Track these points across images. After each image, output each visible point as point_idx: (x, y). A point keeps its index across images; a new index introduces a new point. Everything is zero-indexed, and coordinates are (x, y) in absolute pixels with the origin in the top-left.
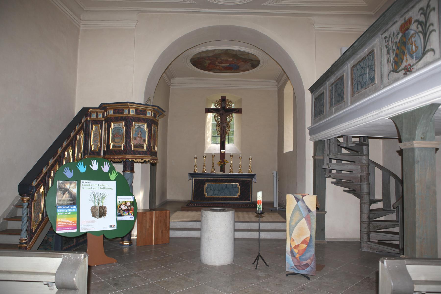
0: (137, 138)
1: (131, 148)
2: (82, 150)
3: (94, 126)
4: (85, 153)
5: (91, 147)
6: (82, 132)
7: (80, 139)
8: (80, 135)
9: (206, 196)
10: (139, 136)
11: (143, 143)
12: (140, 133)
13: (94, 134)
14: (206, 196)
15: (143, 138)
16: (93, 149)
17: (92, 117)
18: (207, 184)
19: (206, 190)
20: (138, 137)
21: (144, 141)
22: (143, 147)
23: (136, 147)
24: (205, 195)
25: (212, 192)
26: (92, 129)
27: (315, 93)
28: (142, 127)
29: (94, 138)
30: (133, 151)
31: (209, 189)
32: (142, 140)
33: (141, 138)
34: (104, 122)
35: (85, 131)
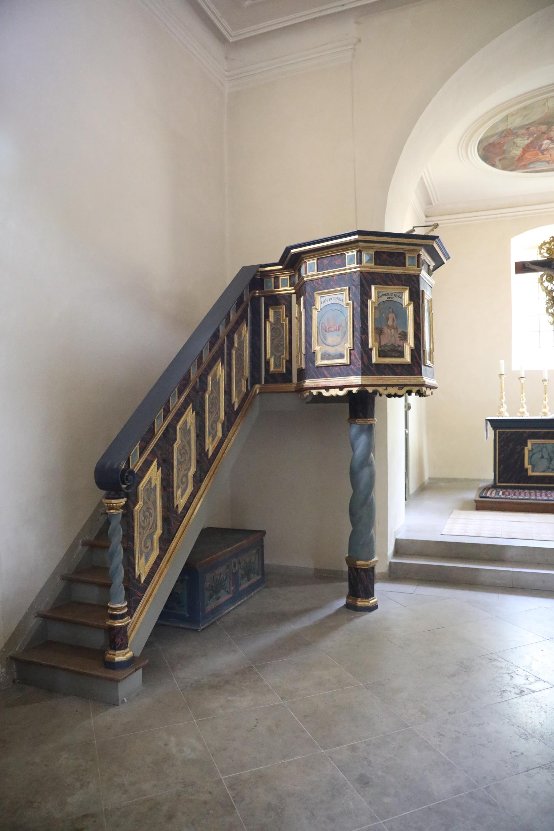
0: (386, 330)
1: (370, 358)
2: (247, 372)
3: (271, 312)
4: (254, 379)
5: (267, 363)
6: (245, 327)
7: (241, 343)
8: (240, 335)
9: (530, 473)
10: (390, 323)
11: (400, 343)
12: (391, 316)
13: (272, 330)
14: (530, 473)
15: (400, 330)
16: (272, 368)
17: (266, 290)
18: (530, 442)
19: (530, 458)
20: (388, 326)
21: (404, 336)
22: (401, 354)
23: (382, 353)
24: (527, 470)
25: (544, 463)
26: (267, 317)
27: (399, 346)
28: (397, 299)
29: (272, 340)
30: (376, 365)
31: (537, 456)
32: (397, 336)
33: (397, 329)
34: (294, 297)
35: (253, 324)
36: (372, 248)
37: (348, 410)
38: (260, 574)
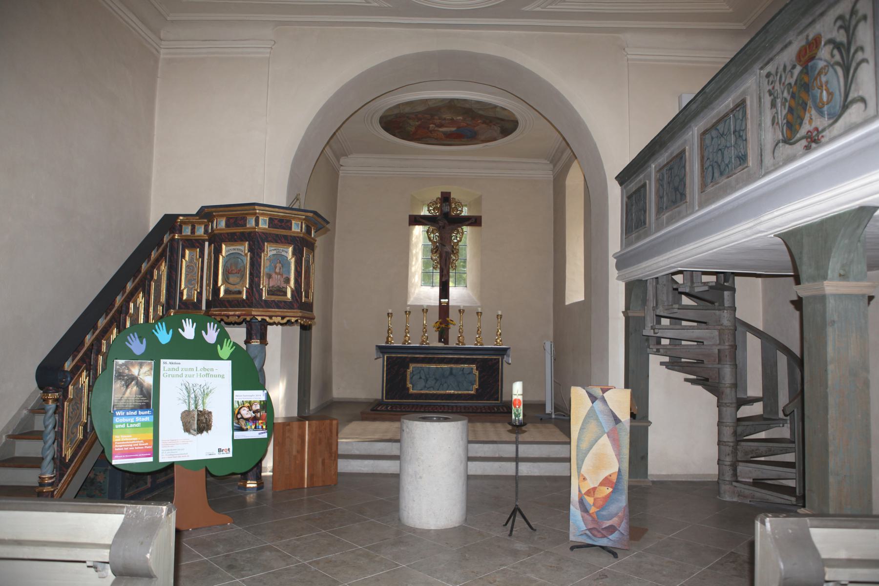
0: (274, 275)
1: (261, 296)
3: (187, 252)
4: (168, 306)
5: (181, 293)
6: (163, 264)
7: (159, 277)
8: (159, 270)
9: (411, 391)
10: (277, 270)
11: (284, 285)
12: (279, 265)
13: (187, 266)
14: (411, 391)
15: (285, 276)
16: (185, 297)
19: (411, 378)
20: (276, 273)
21: (287, 281)
22: (285, 294)
23: (270, 292)
25: (422, 383)
26: (183, 256)
28: (283, 253)
29: (186, 275)
30: (265, 301)
31: (416, 377)
32: (282, 280)
34: (207, 244)
35: (170, 261)
36: (267, 215)
37: (333, 330)
38: (273, 298)
